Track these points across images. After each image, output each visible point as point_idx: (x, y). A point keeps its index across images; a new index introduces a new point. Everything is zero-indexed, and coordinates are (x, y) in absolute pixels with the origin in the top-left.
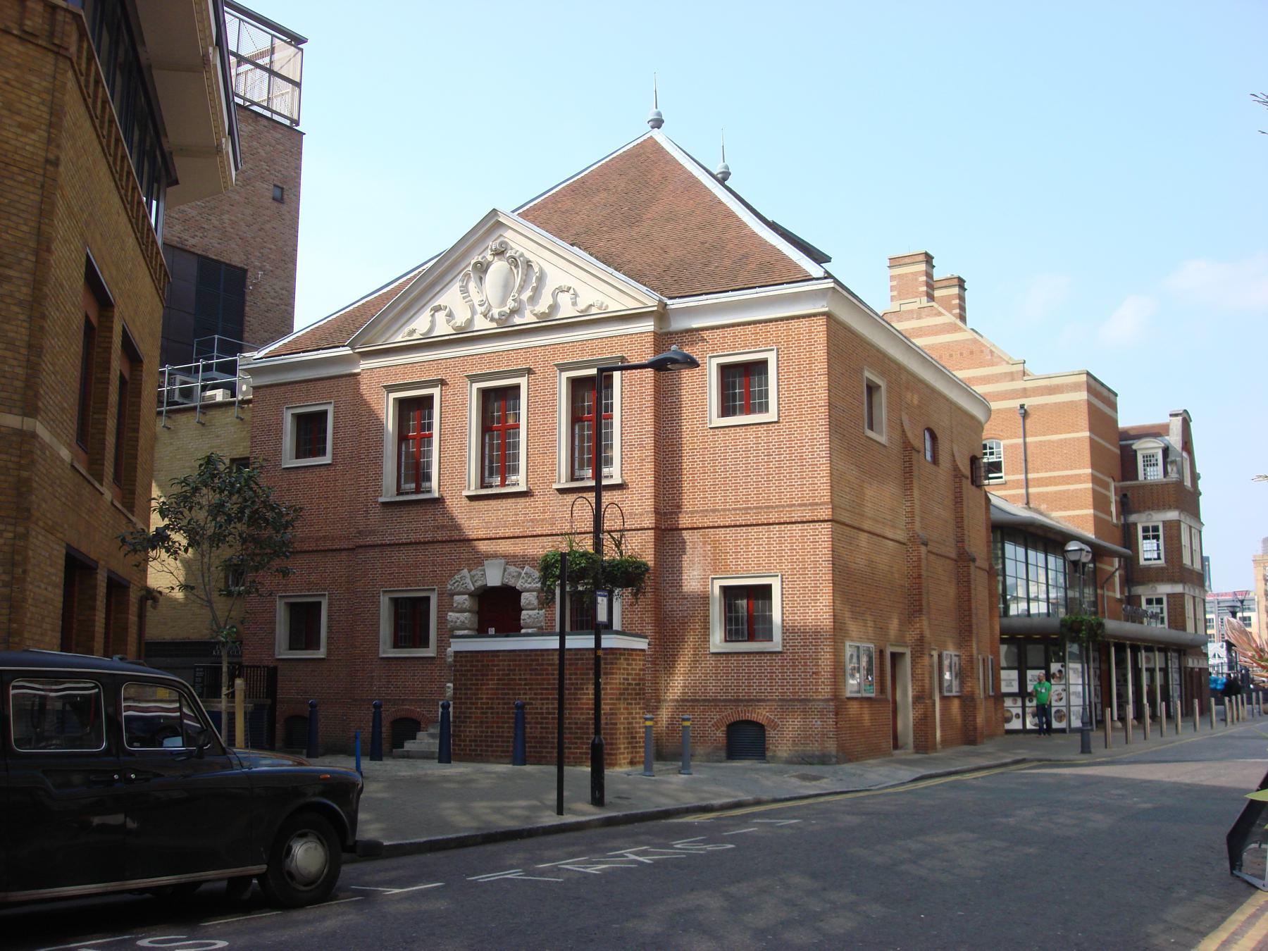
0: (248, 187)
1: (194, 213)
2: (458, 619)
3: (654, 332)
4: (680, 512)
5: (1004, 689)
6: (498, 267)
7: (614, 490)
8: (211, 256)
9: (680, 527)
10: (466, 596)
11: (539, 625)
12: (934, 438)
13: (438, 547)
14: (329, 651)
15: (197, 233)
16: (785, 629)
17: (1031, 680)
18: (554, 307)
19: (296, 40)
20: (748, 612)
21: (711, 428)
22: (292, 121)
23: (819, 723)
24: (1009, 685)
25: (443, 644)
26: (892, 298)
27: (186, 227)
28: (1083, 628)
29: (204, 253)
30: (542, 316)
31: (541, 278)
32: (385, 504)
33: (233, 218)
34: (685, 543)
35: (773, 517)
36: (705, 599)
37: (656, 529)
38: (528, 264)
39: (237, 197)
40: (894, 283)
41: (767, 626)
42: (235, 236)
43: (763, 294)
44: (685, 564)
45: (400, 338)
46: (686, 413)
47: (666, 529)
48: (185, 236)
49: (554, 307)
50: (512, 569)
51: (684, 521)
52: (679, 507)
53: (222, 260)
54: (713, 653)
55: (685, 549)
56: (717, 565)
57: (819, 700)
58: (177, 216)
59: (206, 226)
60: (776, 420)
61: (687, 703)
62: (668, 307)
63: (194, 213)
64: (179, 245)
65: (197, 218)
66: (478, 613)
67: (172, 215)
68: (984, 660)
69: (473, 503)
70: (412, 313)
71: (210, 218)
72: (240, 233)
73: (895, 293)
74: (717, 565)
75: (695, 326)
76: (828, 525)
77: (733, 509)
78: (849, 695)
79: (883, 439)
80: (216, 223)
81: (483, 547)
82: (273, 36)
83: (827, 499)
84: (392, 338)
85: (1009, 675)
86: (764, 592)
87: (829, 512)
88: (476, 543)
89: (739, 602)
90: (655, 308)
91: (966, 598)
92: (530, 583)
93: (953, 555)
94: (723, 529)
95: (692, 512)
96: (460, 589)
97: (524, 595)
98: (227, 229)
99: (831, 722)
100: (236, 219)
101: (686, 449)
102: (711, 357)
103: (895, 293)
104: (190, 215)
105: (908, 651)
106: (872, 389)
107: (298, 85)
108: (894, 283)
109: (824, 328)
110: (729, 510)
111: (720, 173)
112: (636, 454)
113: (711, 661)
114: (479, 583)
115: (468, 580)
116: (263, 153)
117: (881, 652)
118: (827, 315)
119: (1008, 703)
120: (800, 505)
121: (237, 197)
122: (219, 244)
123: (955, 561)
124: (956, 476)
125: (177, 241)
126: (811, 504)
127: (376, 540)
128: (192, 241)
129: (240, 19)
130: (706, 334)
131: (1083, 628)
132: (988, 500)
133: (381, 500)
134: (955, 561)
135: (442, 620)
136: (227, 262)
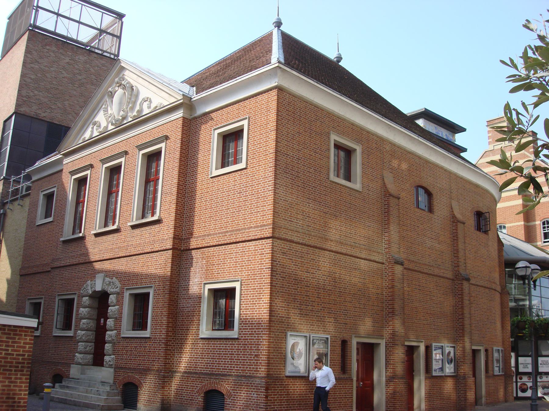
0: (82, 88)
1: (46, 100)
2: (83, 312)
3: (183, 117)
4: (192, 237)
5: (521, 370)
6: (120, 92)
7: (156, 224)
8: (55, 122)
9: (191, 247)
10: (87, 298)
11: (115, 316)
12: (429, 194)
13: (80, 266)
14: (41, 333)
15: (47, 111)
16: (242, 322)
17: (541, 364)
18: (140, 111)
19: (120, 16)
20: (225, 309)
21: (211, 178)
22: (115, 55)
23: (255, 395)
24: (526, 366)
25: (76, 330)
26: (489, 143)
27: (40, 107)
28: (527, 326)
29: (50, 121)
30: (135, 118)
31: (137, 96)
32: (65, 242)
33: (71, 103)
34: (193, 259)
35: (240, 238)
36: (199, 298)
37: (173, 249)
38: (132, 87)
39: (75, 93)
40: (490, 135)
41: (232, 319)
42: (72, 112)
43: (240, 80)
44: (192, 274)
45: (80, 142)
46: (200, 169)
47: (184, 250)
48: (38, 112)
49: (140, 111)
50: (107, 279)
51: (193, 243)
52: (192, 234)
53: (63, 124)
54: (202, 338)
55: (192, 263)
56: (208, 274)
57: (258, 377)
58: (34, 102)
59: (53, 107)
60: (245, 167)
61: (188, 374)
62: (192, 100)
63: (46, 100)
64: (35, 116)
65: (48, 103)
66: (97, 308)
67: (31, 101)
68: (486, 351)
69: (97, 239)
70: (85, 128)
71: (56, 103)
72: (75, 111)
73: (491, 140)
74: (208, 274)
75: (207, 110)
76: (269, 241)
77: (219, 233)
78: (288, 374)
79: (357, 186)
80: (60, 105)
81: (97, 266)
82: (103, 13)
83: (270, 221)
84: (73, 143)
85: (525, 361)
86: (230, 293)
87: (270, 231)
88: (95, 264)
89: (221, 301)
90: (182, 101)
91: (460, 306)
92: (113, 289)
93: (450, 275)
94: (212, 248)
95: (197, 237)
96: (85, 293)
97: (111, 296)
98: (67, 109)
99: (263, 395)
100: (73, 104)
101: (198, 193)
102: (215, 129)
103: (491, 140)
104: (43, 101)
105: (383, 343)
106: (349, 152)
107: (119, 37)
108: (490, 135)
109: (276, 97)
110: (216, 234)
111: (335, 58)
112: (168, 199)
113: (201, 344)
114: (93, 289)
115: (89, 288)
116: (92, 70)
117: (344, 344)
118: (280, 89)
119: (525, 379)
120: (255, 227)
121: (75, 93)
122: (61, 116)
123: (453, 280)
124: (453, 222)
125: (34, 115)
126: (261, 226)
127: (63, 263)
128: (43, 115)
129: (82, 5)
130: (213, 115)
131: (527, 326)
132: (500, 243)
133: (62, 239)
134: (453, 280)
135: (77, 314)
136: (66, 125)
